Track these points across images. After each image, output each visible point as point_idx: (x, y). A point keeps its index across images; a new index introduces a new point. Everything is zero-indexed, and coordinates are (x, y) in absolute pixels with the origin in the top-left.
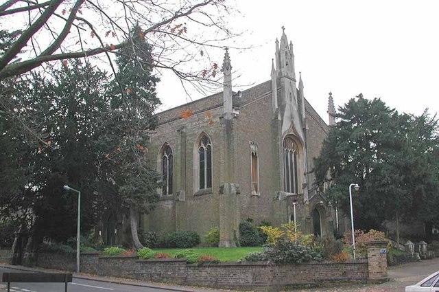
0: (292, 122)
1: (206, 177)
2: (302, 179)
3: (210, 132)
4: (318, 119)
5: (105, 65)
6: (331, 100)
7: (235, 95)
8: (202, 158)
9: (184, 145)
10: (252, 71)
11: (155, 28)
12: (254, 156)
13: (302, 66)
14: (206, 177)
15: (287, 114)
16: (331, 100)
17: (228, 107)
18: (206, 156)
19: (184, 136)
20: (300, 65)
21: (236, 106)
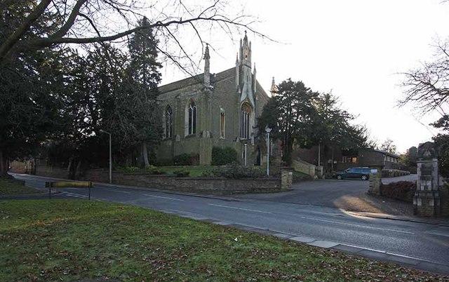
0: (248, 95)
1: (193, 124)
2: (251, 130)
3: (196, 99)
4: (265, 95)
5: (122, 47)
6: (273, 82)
7: (211, 76)
8: (190, 115)
9: (179, 107)
10: (223, 62)
11: (159, 24)
12: (222, 115)
13: (256, 59)
14: (193, 124)
15: (244, 89)
16: (273, 82)
17: (207, 79)
18: (193, 115)
19: (179, 101)
20: (255, 59)
21: (212, 83)
